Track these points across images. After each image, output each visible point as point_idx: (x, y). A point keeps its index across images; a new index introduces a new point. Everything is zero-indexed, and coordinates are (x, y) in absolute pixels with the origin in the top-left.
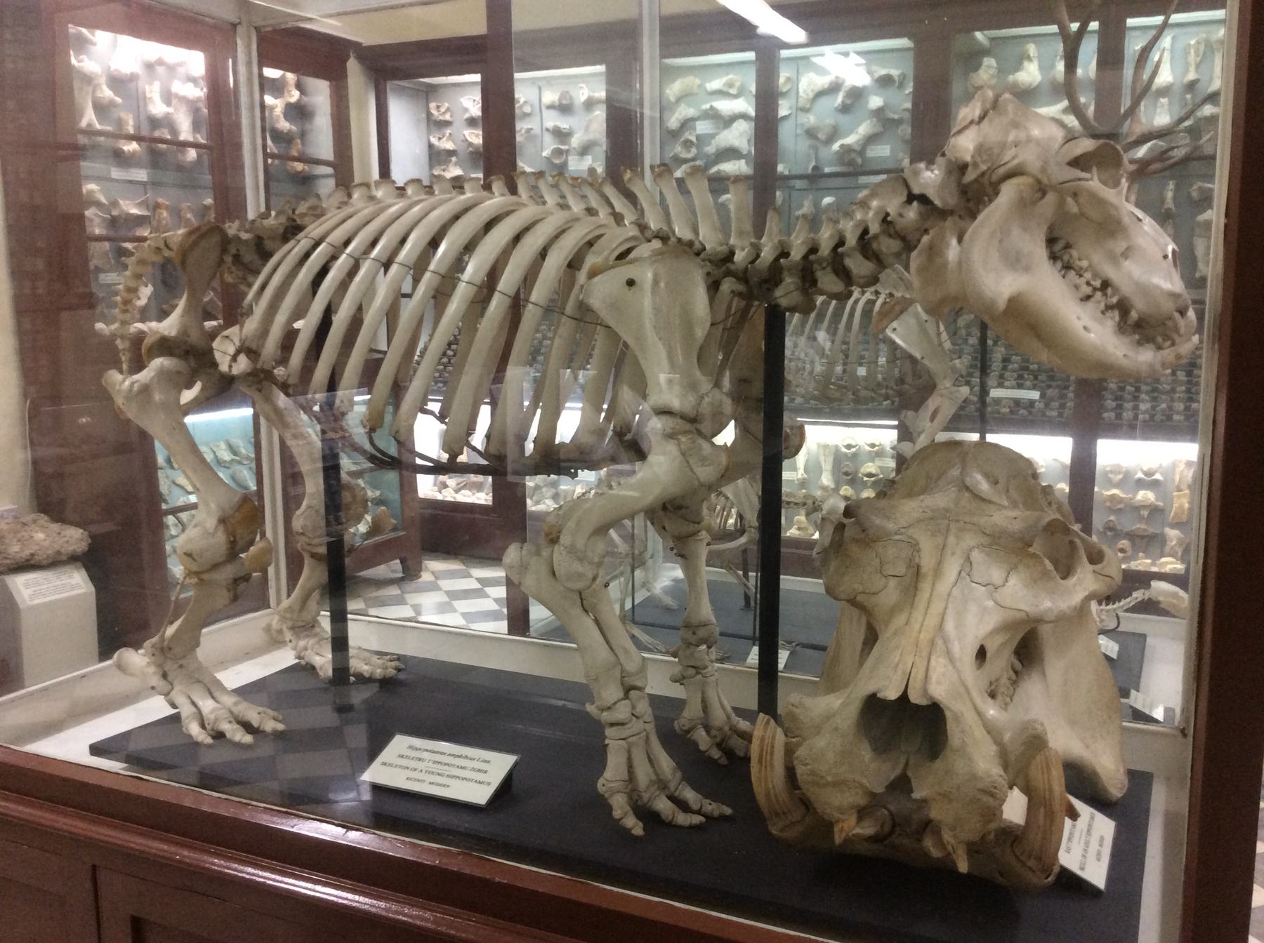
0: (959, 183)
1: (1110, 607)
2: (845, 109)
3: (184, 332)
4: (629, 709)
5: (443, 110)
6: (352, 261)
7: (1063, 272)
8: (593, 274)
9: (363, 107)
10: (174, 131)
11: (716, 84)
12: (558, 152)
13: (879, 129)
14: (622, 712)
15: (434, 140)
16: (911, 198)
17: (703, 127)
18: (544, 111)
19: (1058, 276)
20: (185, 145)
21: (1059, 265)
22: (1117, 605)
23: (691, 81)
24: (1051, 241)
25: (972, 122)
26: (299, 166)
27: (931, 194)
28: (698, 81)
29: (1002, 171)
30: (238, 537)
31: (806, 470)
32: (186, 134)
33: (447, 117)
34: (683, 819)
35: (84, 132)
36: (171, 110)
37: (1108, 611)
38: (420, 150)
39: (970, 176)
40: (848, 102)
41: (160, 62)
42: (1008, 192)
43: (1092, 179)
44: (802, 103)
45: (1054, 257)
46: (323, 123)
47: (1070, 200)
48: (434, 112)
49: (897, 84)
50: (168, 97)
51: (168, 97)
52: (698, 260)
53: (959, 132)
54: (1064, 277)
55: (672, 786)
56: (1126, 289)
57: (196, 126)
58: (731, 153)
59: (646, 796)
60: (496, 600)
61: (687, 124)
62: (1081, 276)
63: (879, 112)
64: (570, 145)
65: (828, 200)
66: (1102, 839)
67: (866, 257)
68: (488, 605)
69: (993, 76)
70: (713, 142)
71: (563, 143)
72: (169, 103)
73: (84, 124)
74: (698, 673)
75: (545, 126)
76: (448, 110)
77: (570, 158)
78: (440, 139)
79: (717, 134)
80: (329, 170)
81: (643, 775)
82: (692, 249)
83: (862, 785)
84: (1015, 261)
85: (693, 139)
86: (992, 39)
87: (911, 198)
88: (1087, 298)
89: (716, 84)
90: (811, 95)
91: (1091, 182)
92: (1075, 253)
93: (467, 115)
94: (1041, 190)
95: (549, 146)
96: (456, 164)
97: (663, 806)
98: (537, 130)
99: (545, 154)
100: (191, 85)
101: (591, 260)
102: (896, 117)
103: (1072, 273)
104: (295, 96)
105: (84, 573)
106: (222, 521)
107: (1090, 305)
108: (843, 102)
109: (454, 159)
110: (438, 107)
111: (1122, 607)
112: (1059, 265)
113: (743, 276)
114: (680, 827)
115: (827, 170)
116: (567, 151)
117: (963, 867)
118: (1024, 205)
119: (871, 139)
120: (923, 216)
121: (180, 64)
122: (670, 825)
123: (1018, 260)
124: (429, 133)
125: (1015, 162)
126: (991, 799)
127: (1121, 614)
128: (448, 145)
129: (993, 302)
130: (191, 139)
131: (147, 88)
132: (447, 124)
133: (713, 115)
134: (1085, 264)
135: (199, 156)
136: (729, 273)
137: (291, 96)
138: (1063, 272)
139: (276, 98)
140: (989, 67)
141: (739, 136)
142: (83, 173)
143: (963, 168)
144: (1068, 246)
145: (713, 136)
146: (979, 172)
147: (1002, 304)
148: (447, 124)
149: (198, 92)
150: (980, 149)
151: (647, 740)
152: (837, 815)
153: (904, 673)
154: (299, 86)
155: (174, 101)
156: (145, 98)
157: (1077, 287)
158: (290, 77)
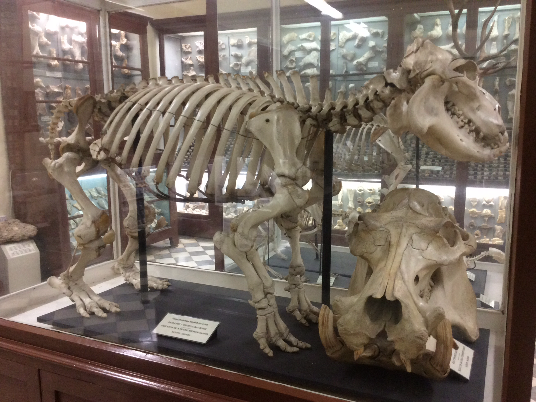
0: (407, 78)
1: (472, 259)
2: (359, 46)
3: (77, 142)
4: (267, 302)
5: (187, 47)
6: (149, 111)
7: (452, 116)
8: (251, 117)
9: (153, 46)
10: (73, 56)
11: (304, 36)
12: (237, 65)
13: (373, 55)
14: (264, 304)
15: (184, 60)
16: (387, 84)
17: (298, 54)
18: (231, 48)
19: (449, 118)
20: (78, 62)
21: (450, 113)
22: (474, 258)
23: (293, 35)
24: (446, 103)
25: (413, 52)
26: (126, 71)
27: (396, 83)
28: (296, 35)
29: (425, 73)
30: (100, 229)
31: (342, 201)
32: (78, 57)
33: (189, 50)
34: (290, 349)
35: (35, 56)
36: (72, 47)
37: (470, 260)
38: (178, 64)
39: (412, 75)
40: (360, 43)
41: (67, 27)
42: (428, 82)
43: (464, 76)
44: (340, 44)
45: (447, 110)
46: (136, 53)
47: (454, 85)
48: (184, 48)
49: (381, 36)
50: (70, 42)
51: (70, 42)
52: (296, 111)
53: (407, 56)
54: (452, 118)
55: (285, 335)
56: (478, 123)
57: (82, 54)
58: (310, 65)
59: (274, 339)
60: (210, 256)
61: (291, 53)
62: (459, 118)
63: (373, 48)
64: (241, 62)
65: (351, 85)
66: (468, 358)
67: (368, 110)
68: (207, 258)
69: (421, 33)
70: (303, 60)
71: (239, 61)
72: (71, 44)
73: (34, 53)
74: (296, 287)
75: (231, 54)
76: (190, 47)
77: (242, 67)
78: (186, 59)
79: (304, 57)
80: (139, 73)
81: (273, 330)
82: (293, 106)
83: (366, 335)
84: (431, 111)
85: (294, 59)
86: (421, 17)
87: (387, 84)
88: (462, 127)
89: (304, 36)
90: (344, 41)
91: (463, 78)
92: (456, 108)
93: (198, 49)
94: (442, 81)
95: (233, 62)
96: (193, 70)
97: (281, 343)
98: (228, 55)
99: (231, 66)
100: (80, 36)
101: (250, 111)
102: (380, 50)
103: (455, 116)
104: (124, 41)
105: (35, 244)
106: (94, 222)
107: (463, 130)
108: (358, 43)
109: (192, 68)
110: (185, 46)
111: (477, 259)
112: (450, 113)
113: (315, 118)
114: (289, 353)
115: (351, 73)
116: (241, 65)
117: (409, 369)
118: (435, 88)
119: (370, 59)
120: (392, 92)
121: (76, 28)
122: (285, 352)
123: (432, 111)
124: (182, 57)
125: (431, 69)
126: (421, 341)
127: (476, 262)
128: (190, 62)
129: (422, 129)
130: (80, 59)
131: (62, 37)
132: (189, 53)
133: (302, 49)
134: (461, 112)
135: (84, 66)
136: (309, 117)
137: (123, 41)
138: (452, 116)
139: (116, 42)
140: (420, 28)
141: (314, 58)
142: (34, 74)
143: (409, 72)
144: (454, 105)
145: (302, 58)
146: (416, 73)
147: (425, 130)
148: (189, 53)
149: (83, 39)
150: (416, 64)
151: (275, 315)
152: (355, 347)
153: (384, 287)
154: (126, 37)
155: (73, 43)
156: (61, 42)
157: (457, 122)
158: (123, 33)
